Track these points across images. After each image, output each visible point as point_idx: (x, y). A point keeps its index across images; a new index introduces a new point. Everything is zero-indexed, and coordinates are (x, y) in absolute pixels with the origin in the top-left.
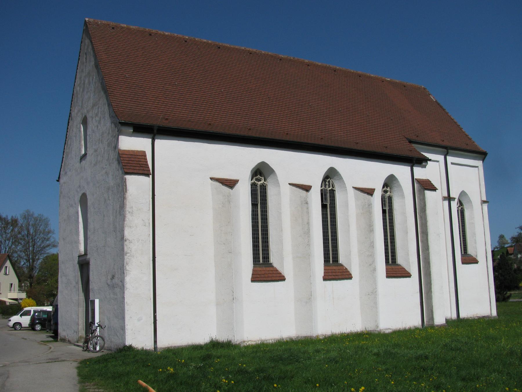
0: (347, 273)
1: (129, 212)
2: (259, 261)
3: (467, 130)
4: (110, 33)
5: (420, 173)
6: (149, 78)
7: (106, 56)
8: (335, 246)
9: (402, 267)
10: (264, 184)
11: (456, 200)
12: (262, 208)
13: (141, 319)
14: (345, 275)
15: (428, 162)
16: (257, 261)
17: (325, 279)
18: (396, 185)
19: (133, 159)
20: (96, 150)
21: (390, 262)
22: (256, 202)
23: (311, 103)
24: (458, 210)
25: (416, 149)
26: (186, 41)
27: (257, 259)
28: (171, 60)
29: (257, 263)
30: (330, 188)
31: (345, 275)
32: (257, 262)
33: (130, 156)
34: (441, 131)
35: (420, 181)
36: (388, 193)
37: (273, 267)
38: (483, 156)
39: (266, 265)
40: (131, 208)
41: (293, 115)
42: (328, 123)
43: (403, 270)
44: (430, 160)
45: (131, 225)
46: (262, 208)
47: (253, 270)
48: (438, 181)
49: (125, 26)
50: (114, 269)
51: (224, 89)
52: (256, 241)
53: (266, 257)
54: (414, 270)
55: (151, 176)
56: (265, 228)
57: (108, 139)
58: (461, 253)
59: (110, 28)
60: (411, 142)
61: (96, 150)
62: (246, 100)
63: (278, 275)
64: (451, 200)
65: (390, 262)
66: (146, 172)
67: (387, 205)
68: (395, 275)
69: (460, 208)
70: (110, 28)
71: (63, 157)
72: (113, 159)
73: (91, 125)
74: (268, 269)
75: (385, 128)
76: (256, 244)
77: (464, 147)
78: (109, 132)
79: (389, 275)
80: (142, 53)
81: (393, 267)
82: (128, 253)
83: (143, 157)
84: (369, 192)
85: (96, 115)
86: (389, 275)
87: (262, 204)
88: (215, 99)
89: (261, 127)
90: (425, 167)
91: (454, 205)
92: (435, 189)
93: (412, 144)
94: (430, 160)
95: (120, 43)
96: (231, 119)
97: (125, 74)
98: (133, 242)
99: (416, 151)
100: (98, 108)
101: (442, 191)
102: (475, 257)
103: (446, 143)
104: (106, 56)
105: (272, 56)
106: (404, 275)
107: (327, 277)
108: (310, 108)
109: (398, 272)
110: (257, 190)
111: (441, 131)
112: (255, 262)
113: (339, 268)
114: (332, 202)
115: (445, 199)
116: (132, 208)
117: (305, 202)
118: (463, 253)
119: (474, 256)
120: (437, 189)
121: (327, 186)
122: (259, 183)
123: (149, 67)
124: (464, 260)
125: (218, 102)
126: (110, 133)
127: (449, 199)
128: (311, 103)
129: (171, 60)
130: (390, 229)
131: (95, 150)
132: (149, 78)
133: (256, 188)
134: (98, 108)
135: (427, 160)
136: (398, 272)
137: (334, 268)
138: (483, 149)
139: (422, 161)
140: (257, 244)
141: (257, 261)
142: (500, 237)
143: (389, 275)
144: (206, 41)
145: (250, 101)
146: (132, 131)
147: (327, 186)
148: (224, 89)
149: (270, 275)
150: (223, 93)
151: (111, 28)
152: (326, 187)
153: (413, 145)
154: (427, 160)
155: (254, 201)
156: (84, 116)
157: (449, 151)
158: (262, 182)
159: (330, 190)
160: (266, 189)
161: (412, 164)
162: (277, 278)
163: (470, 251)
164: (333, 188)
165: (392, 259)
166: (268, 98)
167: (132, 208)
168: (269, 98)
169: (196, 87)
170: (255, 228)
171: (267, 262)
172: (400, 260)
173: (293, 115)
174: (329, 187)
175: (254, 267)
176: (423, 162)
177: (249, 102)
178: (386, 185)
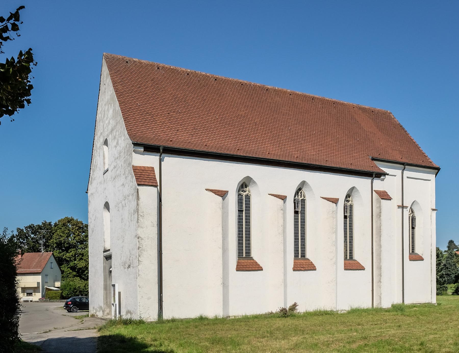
0: (313, 266)
1: (141, 216)
2: (243, 255)
3: (423, 149)
4: (124, 66)
5: (378, 184)
6: (157, 106)
7: (121, 87)
8: (304, 244)
9: (358, 262)
10: (249, 194)
11: (409, 208)
12: (247, 213)
13: (150, 298)
14: (311, 267)
15: (386, 176)
16: (241, 255)
17: (294, 270)
18: (356, 195)
19: (144, 174)
20: (115, 166)
21: (348, 258)
22: (242, 209)
23: (290, 128)
24: (409, 217)
25: (377, 165)
26: (188, 74)
27: (241, 253)
28: (175, 90)
29: (241, 257)
30: (302, 198)
31: (311, 267)
32: (241, 256)
33: (141, 171)
34: (401, 150)
35: (378, 192)
36: (350, 202)
37: (253, 260)
38: (437, 171)
39: (248, 258)
40: (142, 212)
41: (237, 143)
42: (303, 144)
43: (361, 266)
44: (388, 174)
45: (143, 226)
46: (247, 213)
47: (238, 262)
48: (395, 194)
49: (137, 60)
50: (130, 260)
51: (218, 116)
52: (241, 239)
53: (248, 252)
54: (367, 264)
55: (159, 187)
56: (248, 229)
57: (124, 157)
58: (409, 252)
59: (124, 62)
60: (373, 159)
61: (115, 166)
62: (237, 125)
63: (257, 266)
64: (404, 208)
65: (348, 258)
66: (154, 184)
67: (349, 211)
68: (351, 268)
69: (411, 215)
70: (124, 62)
71: (90, 173)
72: (128, 173)
73: (111, 146)
74: (249, 261)
75: (323, 149)
76: (240, 242)
77: (420, 163)
78: (125, 151)
79: (347, 268)
80: (151, 84)
81: (351, 262)
82: (140, 248)
83: (152, 172)
84: (334, 201)
85: (114, 138)
86: (347, 268)
87: (247, 211)
88: (211, 124)
89: (248, 148)
90: (383, 180)
91: (407, 212)
92: (391, 198)
93: (373, 161)
94: (388, 174)
95: (133, 75)
96: (223, 141)
97: (137, 103)
98: (144, 239)
99: (377, 167)
100: (116, 132)
101: (397, 200)
102: (421, 256)
103: (404, 160)
104: (121, 87)
105: (260, 87)
106: (359, 268)
107: (296, 269)
108: (289, 132)
109: (354, 266)
110: (242, 200)
111: (401, 150)
112: (240, 256)
113: (306, 261)
114: (303, 209)
115: (399, 207)
116: (143, 212)
117: (281, 209)
118: (411, 252)
119: (421, 255)
120: (392, 199)
121: (299, 197)
122: (245, 194)
123: (157, 96)
124: (411, 258)
125: (213, 126)
126: (126, 152)
127: (403, 207)
128: (290, 128)
129: (175, 90)
130: (350, 231)
131: (114, 166)
132: (157, 106)
133: (242, 197)
134: (116, 132)
135: (385, 174)
136: (354, 266)
137: (302, 261)
138: (436, 165)
139: (380, 175)
140: (242, 242)
141: (241, 255)
142: (449, 242)
143: (346, 268)
144: (204, 74)
145: (240, 126)
146: (143, 150)
147: (299, 197)
148: (218, 116)
149: (251, 266)
150: (218, 119)
151: (125, 62)
152: (298, 197)
153: (375, 162)
154: (385, 174)
155: (240, 208)
156: (105, 139)
157: (406, 166)
158: (247, 193)
159: (302, 200)
160: (250, 198)
161: (372, 178)
162: (257, 269)
163: (417, 251)
164: (304, 198)
165: (350, 256)
166: (255, 123)
167: (143, 212)
168: (256, 124)
169: (196, 114)
170: (240, 230)
171: (249, 256)
172: (356, 256)
173: (237, 143)
174: (301, 197)
175: (238, 260)
176: (382, 176)
177: (239, 127)
178: (348, 196)
